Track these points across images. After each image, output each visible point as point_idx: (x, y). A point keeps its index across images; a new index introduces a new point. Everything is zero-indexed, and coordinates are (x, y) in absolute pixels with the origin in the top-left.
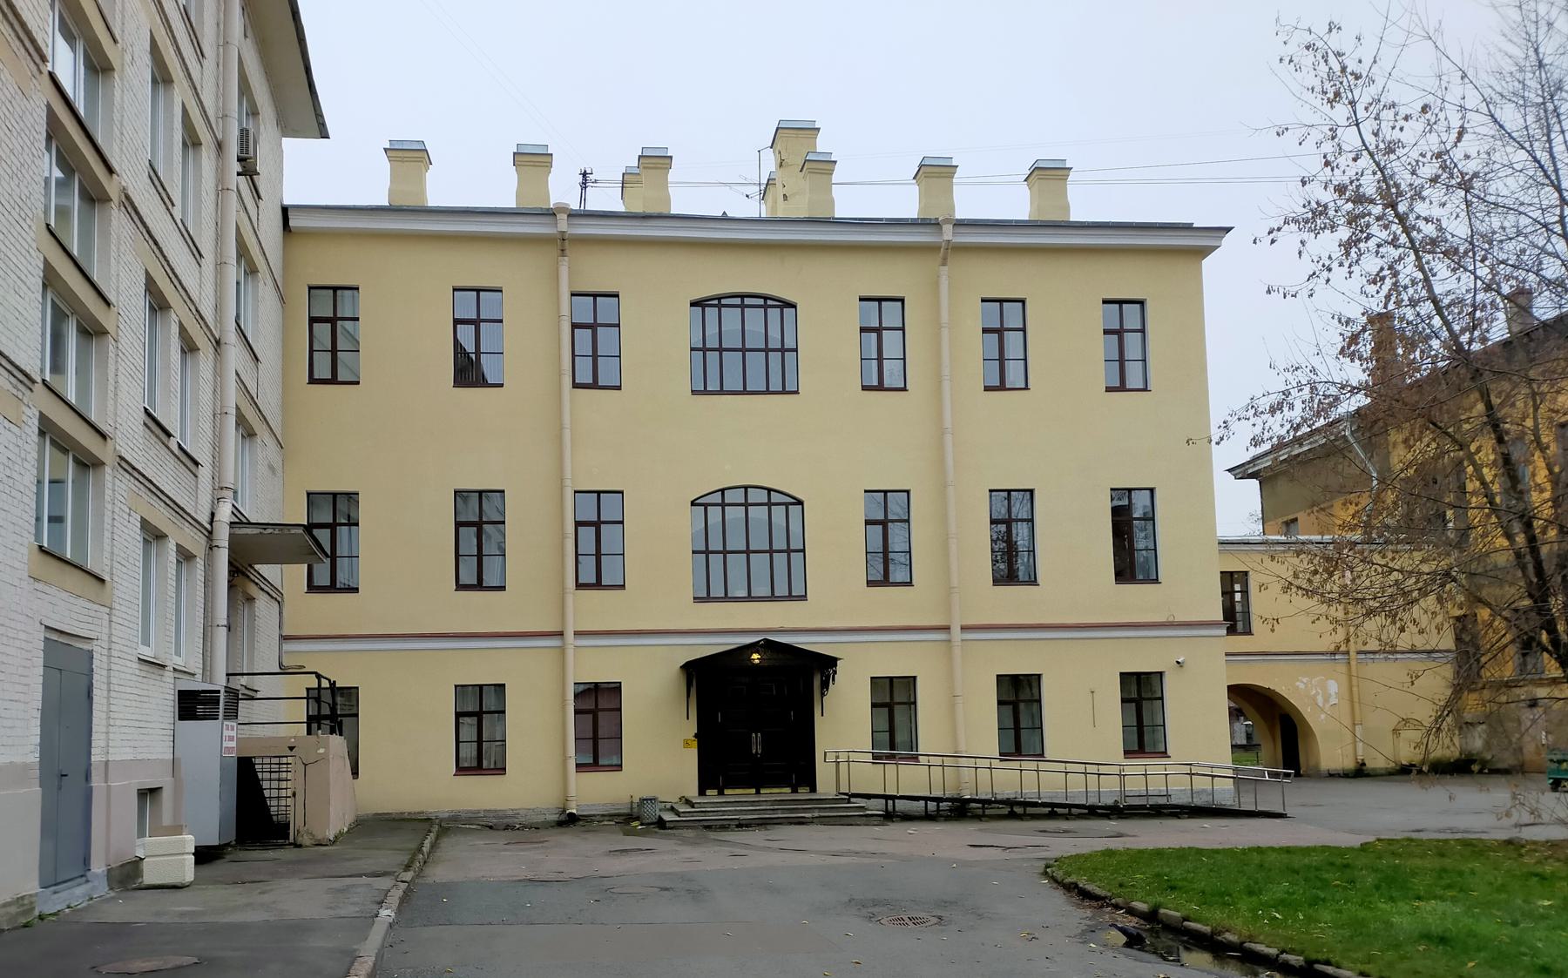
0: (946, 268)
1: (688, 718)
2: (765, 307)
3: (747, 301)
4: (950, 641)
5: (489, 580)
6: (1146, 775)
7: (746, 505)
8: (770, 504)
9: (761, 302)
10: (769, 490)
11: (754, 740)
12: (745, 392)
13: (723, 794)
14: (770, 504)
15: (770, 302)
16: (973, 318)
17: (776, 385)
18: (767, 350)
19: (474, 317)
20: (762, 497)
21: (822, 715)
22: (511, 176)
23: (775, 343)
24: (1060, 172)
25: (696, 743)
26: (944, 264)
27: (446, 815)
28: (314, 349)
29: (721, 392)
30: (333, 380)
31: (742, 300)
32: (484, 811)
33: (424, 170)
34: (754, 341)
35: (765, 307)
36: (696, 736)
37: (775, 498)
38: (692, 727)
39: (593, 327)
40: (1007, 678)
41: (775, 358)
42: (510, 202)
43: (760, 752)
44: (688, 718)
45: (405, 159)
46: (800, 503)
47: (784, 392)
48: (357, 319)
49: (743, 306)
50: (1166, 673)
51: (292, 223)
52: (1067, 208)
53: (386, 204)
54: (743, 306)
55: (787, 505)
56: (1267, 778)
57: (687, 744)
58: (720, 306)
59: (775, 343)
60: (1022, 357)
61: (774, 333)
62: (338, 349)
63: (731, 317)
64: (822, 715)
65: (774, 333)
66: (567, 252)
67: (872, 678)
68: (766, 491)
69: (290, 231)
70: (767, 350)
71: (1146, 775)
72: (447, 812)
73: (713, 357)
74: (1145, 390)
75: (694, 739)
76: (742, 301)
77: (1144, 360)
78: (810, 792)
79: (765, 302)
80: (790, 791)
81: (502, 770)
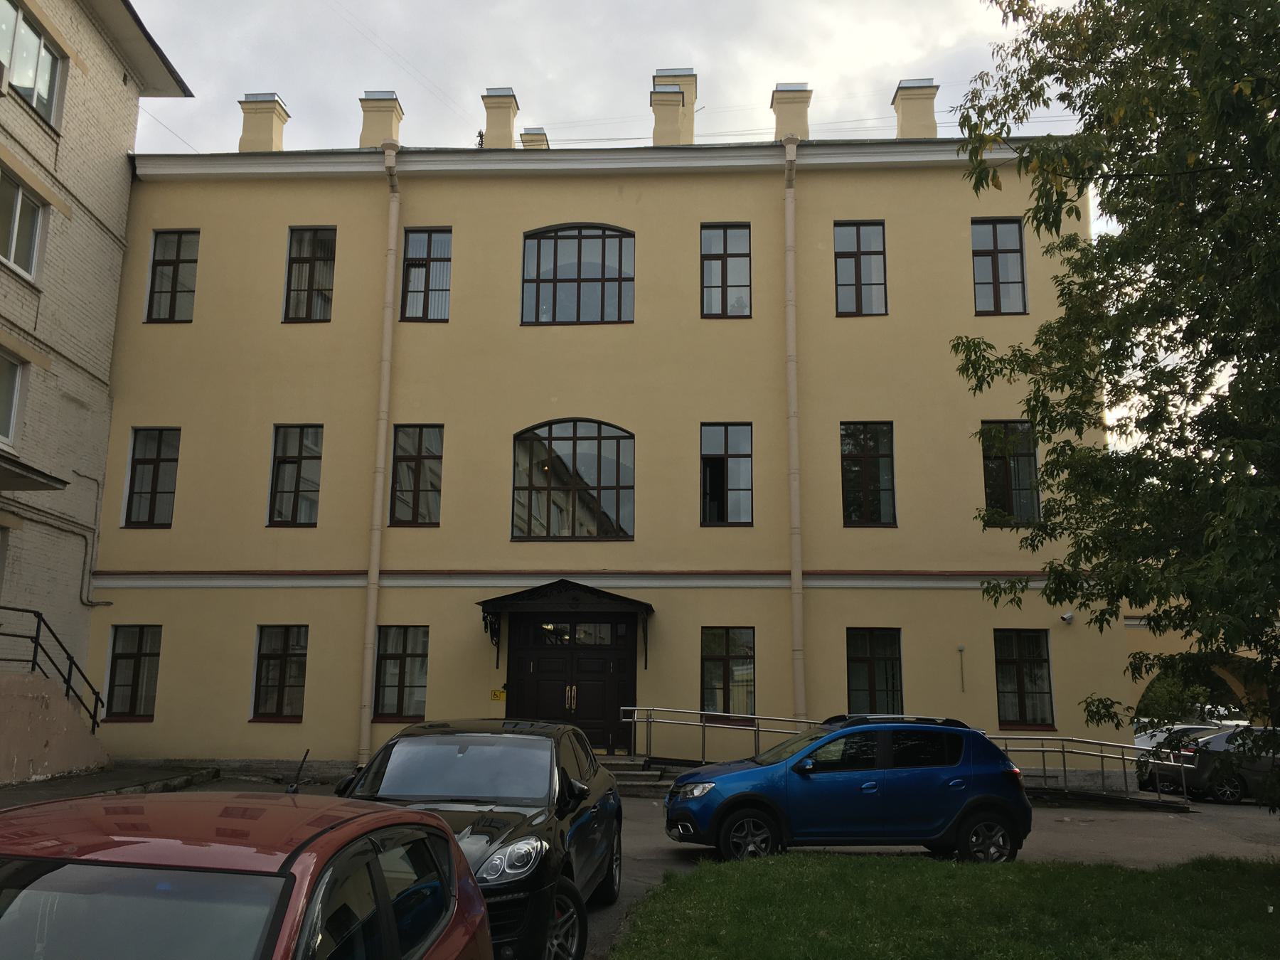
0: (792, 190)
1: (497, 668)
2: (603, 237)
3: (584, 232)
4: (790, 588)
5: (302, 518)
6: (1063, 752)
7: (575, 439)
8: (599, 438)
9: (599, 232)
10: (600, 423)
11: (568, 694)
12: (578, 322)
13: (613, 754)
14: (599, 438)
15: (608, 233)
16: (824, 243)
17: (611, 313)
18: (603, 280)
19: (854, 249)
20: (592, 430)
21: (646, 668)
22: (237, 118)
23: (612, 272)
24: (927, 91)
25: (504, 696)
26: (790, 186)
27: (237, 765)
28: (991, 286)
29: (554, 323)
30: (171, 320)
31: (579, 230)
32: (277, 761)
33: (512, 114)
34: (593, 270)
35: (603, 237)
36: (505, 687)
37: (606, 431)
38: (501, 677)
39: (723, 258)
40: (720, 631)
41: (611, 288)
42: (892, 134)
43: (574, 707)
44: (497, 668)
45: (258, 111)
46: (632, 436)
47: (620, 322)
48: (449, 260)
49: (580, 238)
50: (1051, 630)
51: (139, 172)
52: (934, 127)
53: (237, 151)
54: (580, 238)
55: (618, 439)
56: (1173, 763)
57: (495, 695)
58: (556, 238)
59: (612, 272)
60: (1020, 280)
61: (612, 262)
62: (863, 282)
63: (568, 249)
64: (646, 668)
65: (612, 262)
66: (398, 187)
67: (702, 627)
68: (596, 425)
69: (140, 180)
70: (603, 280)
71: (1063, 752)
72: (239, 761)
73: (546, 289)
74: (1025, 313)
75: (503, 690)
76: (580, 233)
77: (1023, 282)
78: (628, 755)
79: (604, 233)
80: (606, 753)
81: (297, 719)
